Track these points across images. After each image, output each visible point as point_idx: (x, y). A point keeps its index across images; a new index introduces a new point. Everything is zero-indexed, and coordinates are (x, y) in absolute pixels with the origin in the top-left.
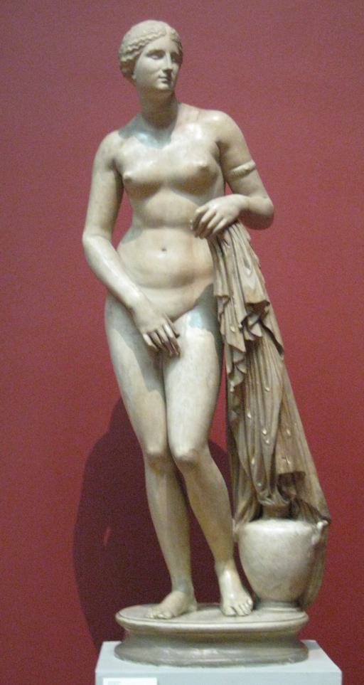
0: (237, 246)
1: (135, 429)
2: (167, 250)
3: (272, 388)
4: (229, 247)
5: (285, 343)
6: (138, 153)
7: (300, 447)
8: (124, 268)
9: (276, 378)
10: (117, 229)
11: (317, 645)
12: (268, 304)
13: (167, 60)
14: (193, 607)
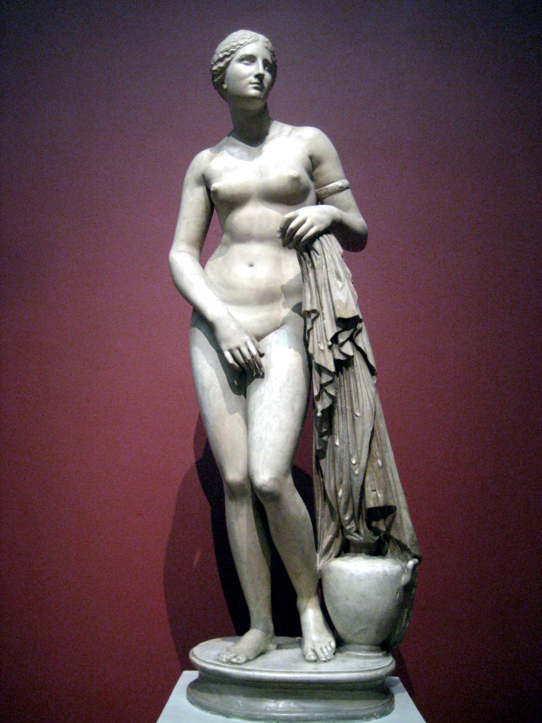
0: (328, 256)
1: (216, 458)
2: (257, 265)
3: (363, 414)
4: (319, 257)
5: (376, 363)
6: (229, 166)
7: (391, 479)
8: (210, 284)
9: (368, 403)
10: (206, 246)
11: (404, 688)
12: (361, 321)
13: (258, 65)
14: (272, 646)
